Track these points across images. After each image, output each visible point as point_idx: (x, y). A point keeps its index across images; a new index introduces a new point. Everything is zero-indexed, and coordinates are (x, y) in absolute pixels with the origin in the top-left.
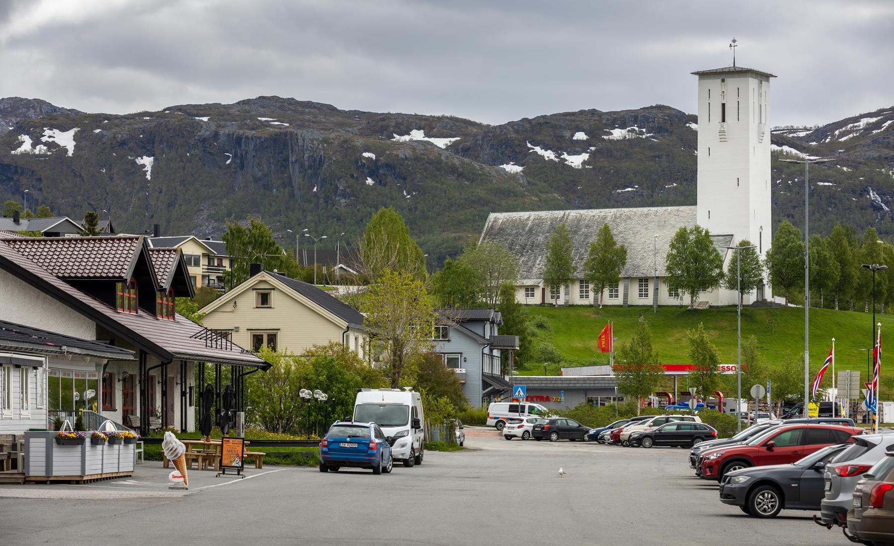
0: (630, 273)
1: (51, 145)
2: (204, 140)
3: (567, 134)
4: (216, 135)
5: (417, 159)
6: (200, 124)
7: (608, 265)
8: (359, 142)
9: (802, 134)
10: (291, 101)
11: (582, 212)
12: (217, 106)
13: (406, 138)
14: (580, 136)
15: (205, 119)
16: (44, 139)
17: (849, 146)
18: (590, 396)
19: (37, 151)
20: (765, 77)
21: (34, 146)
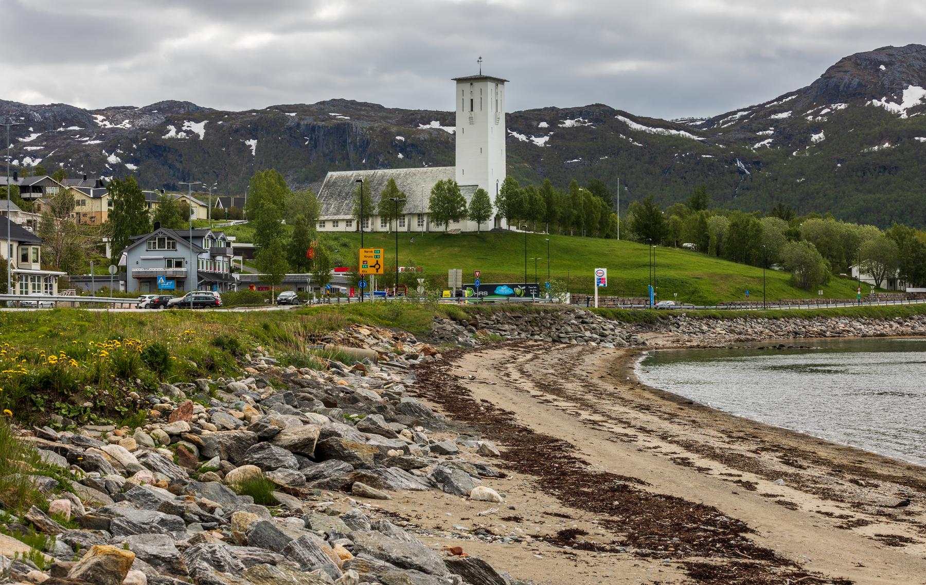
0: (412, 211)
1: (189, 132)
2: (290, 128)
3: (535, 124)
4: (298, 125)
5: (432, 141)
6: (287, 118)
7: (394, 206)
8: (394, 129)
9: (698, 123)
10: (353, 102)
11: (386, 171)
12: (302, 105)
13: (428, 126)
14: (544, 125)
15: (293, 114)
16: (184, 128)
17: (726, 131)
18: (299, 286)
19: (179, 137)
20: (500, 81)
21: (177, 133)
